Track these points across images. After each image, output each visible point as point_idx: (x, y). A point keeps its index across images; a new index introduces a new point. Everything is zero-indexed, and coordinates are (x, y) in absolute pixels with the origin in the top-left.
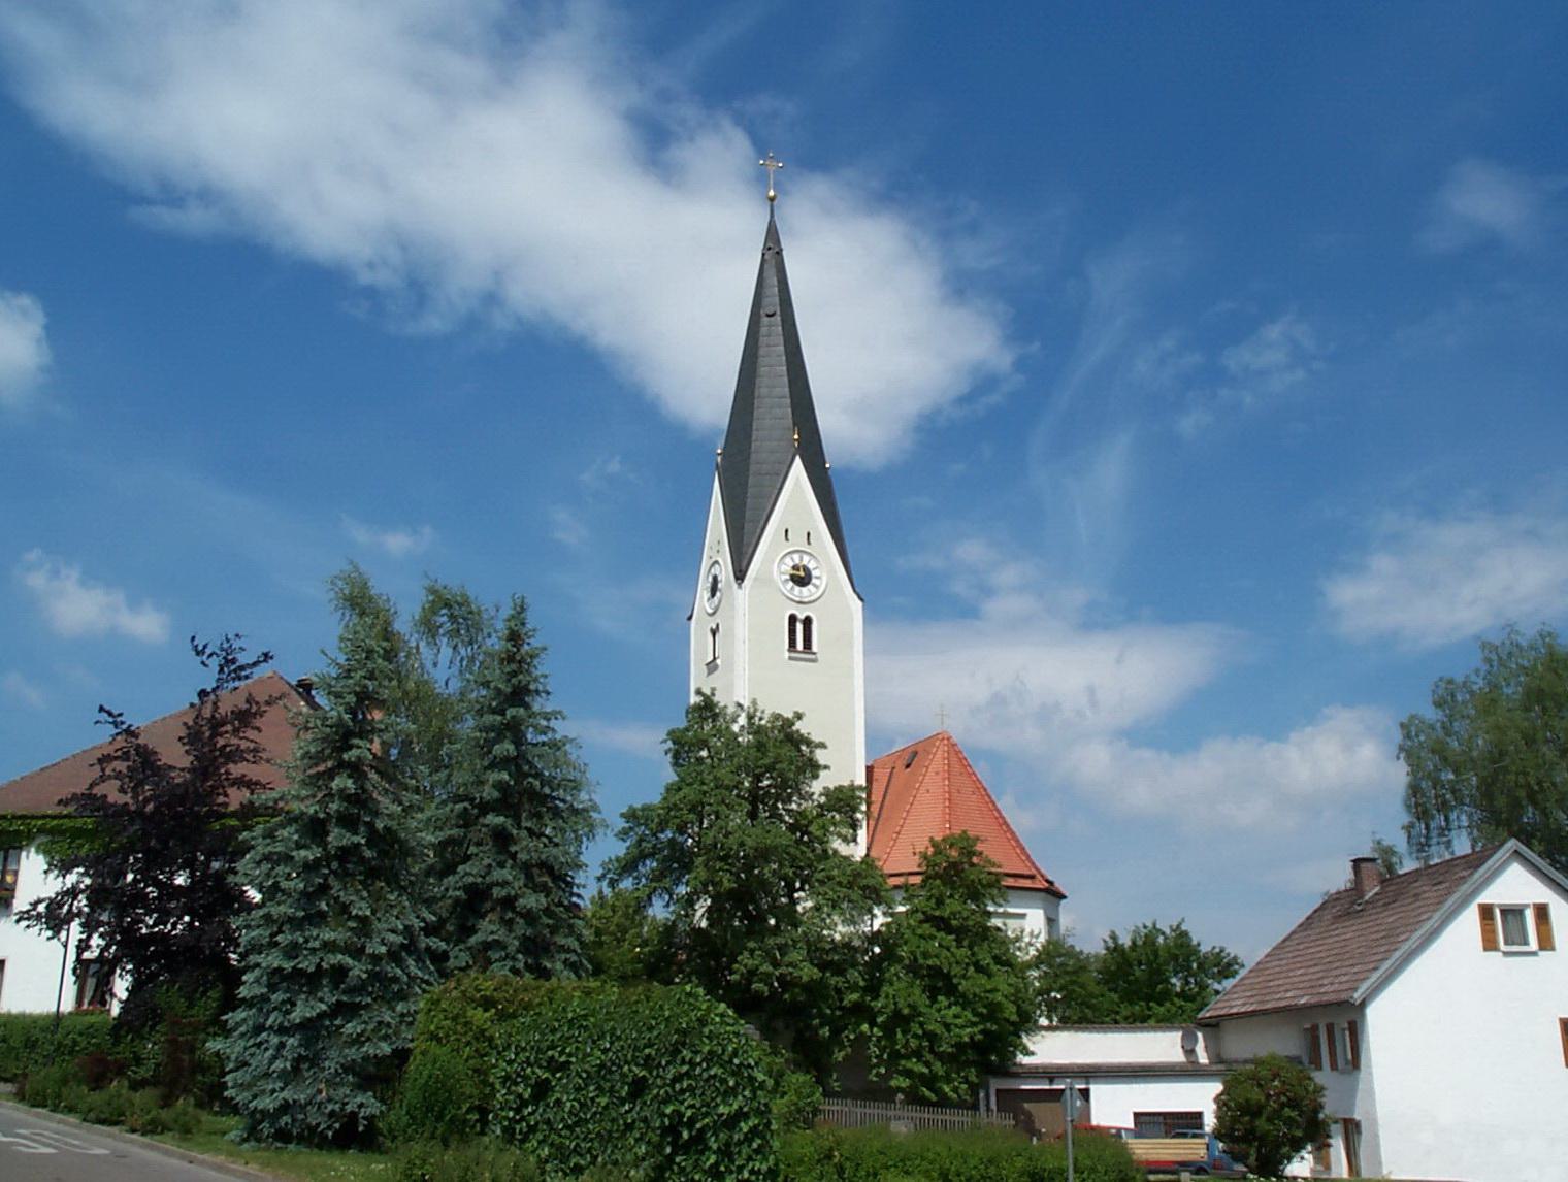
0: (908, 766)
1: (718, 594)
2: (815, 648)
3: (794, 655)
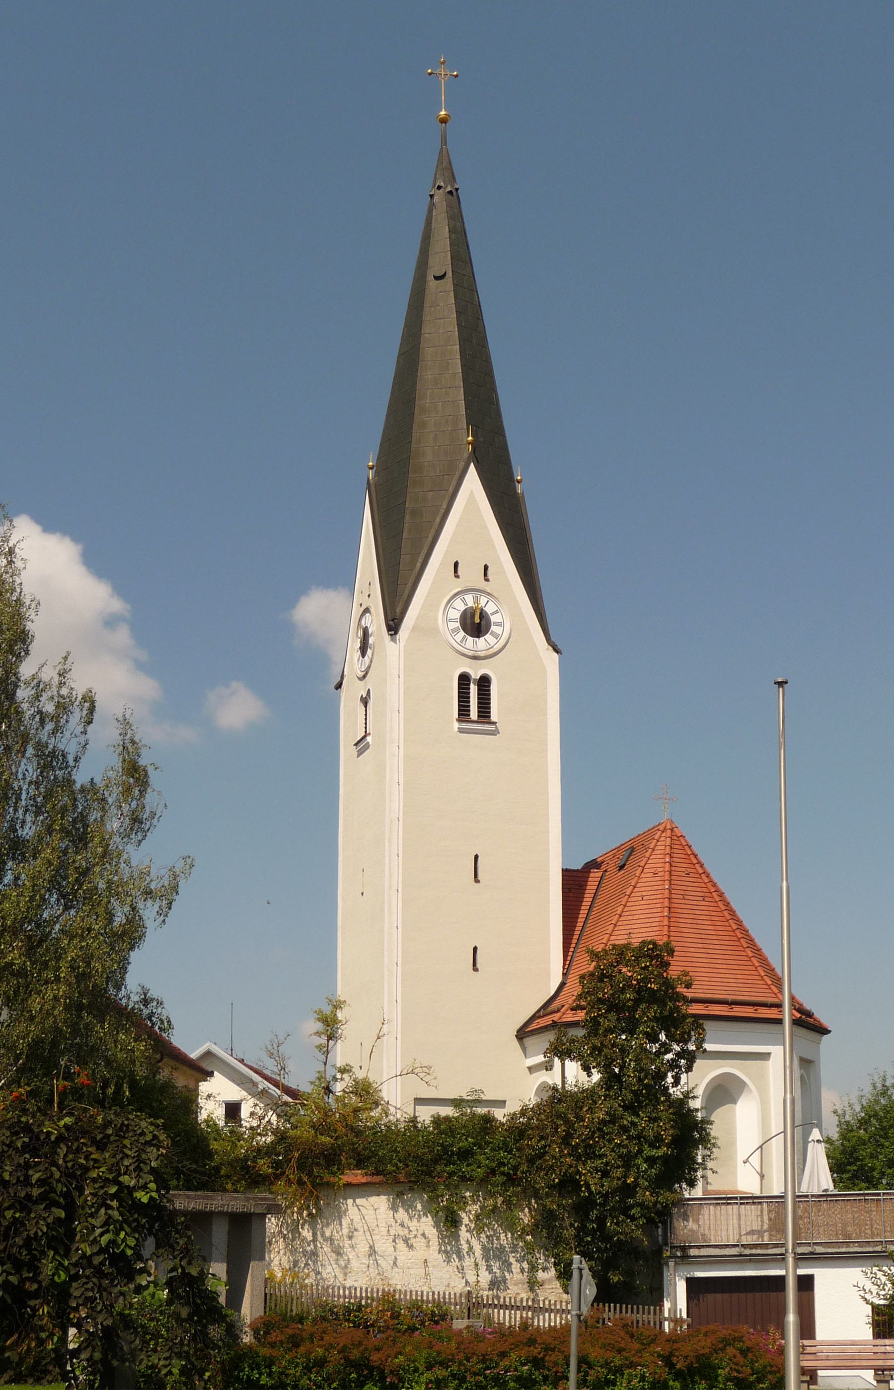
0: (621, 868)
1: (369, 652)
2: (494, 717)
3: (465, 726)
